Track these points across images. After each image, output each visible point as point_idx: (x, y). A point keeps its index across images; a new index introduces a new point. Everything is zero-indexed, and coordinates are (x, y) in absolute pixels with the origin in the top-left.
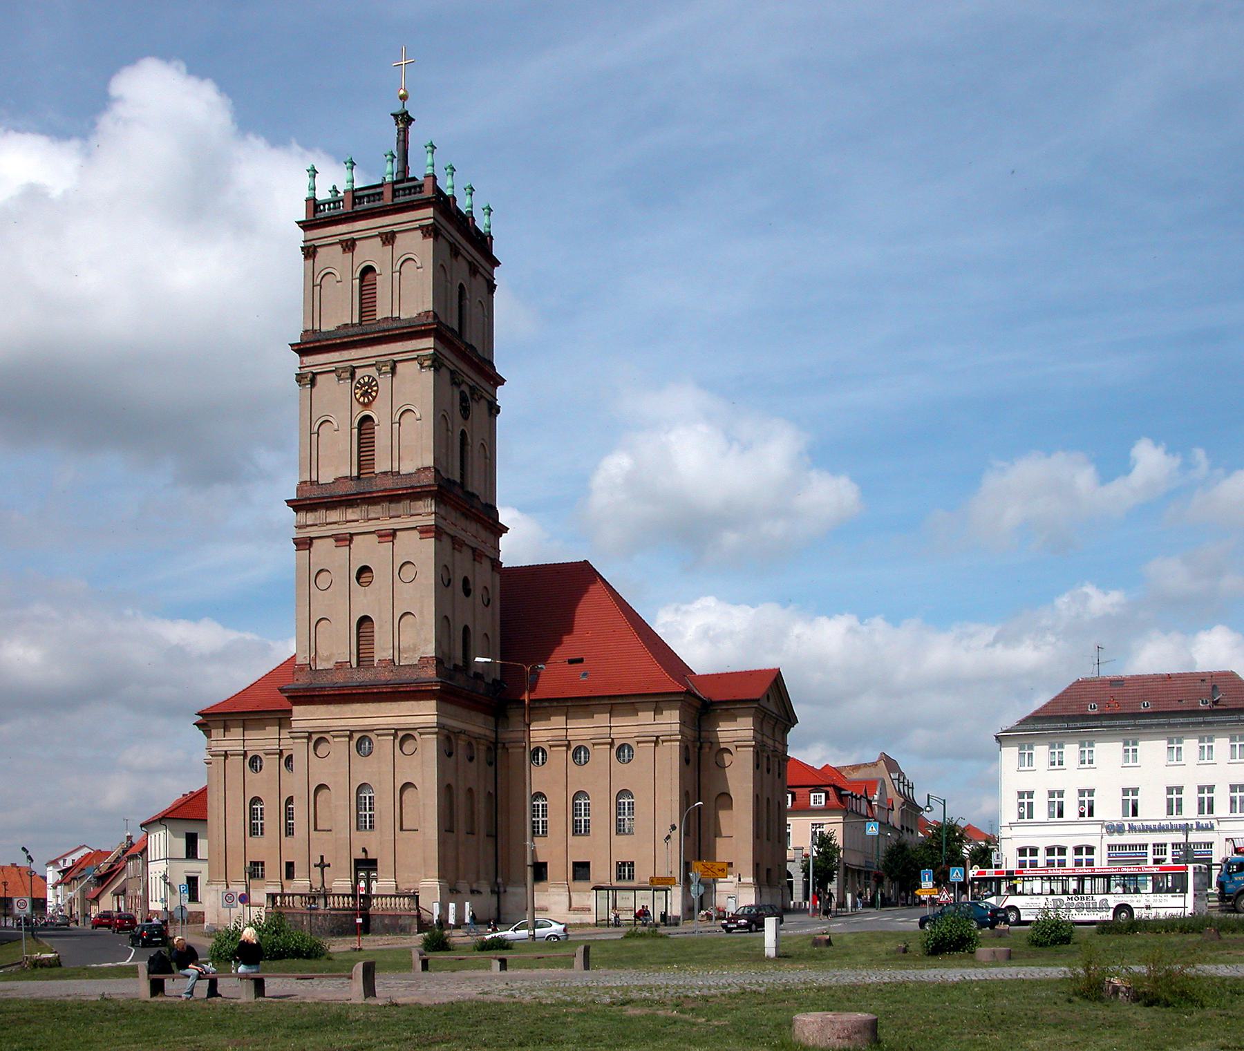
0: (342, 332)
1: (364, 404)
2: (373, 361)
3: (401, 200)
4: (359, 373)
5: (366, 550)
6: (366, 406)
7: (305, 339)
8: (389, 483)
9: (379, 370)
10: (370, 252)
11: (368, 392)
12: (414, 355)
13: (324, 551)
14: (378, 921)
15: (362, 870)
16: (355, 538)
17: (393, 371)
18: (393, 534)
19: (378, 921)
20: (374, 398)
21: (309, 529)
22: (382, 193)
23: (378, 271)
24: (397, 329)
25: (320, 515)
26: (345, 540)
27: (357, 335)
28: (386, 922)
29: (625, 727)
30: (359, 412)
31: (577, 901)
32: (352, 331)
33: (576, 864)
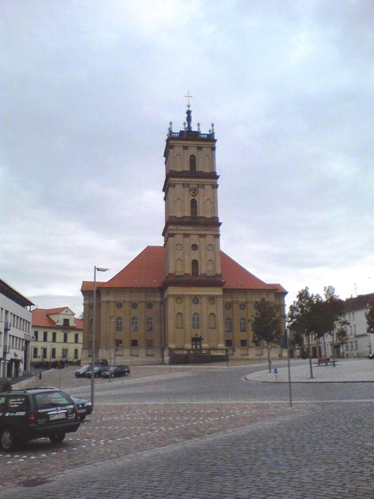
1: (193, 195)
4: (191, 186)
5: (194, 239)
11: (194, 192)
33: (133, 341)
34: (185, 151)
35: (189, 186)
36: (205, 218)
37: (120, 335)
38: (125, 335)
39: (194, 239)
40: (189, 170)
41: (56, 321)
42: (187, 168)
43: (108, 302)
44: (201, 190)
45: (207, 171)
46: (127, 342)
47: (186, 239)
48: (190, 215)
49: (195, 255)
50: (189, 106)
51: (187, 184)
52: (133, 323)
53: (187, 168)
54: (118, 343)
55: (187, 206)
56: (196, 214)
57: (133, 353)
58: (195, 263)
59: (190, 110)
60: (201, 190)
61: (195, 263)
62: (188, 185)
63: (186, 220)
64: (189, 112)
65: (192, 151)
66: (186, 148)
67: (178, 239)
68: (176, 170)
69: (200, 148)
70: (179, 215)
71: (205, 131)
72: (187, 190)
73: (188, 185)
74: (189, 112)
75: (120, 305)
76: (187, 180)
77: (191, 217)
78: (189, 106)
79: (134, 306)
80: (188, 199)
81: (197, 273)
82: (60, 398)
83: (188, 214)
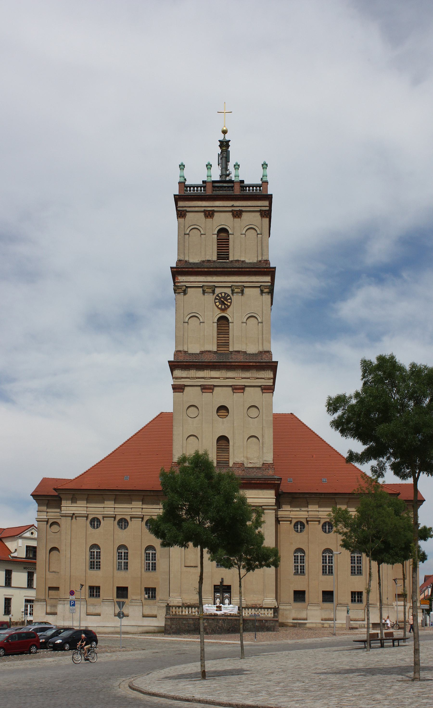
0: (206, 265)
1: (221, 309)
2: (230, 284)
3: (215, 193)
4: (218, 291)
5: (222, 396)
6: (223, 310)
7: (180, 266)
8: (241, 358)
9: (233, 291)
10: (223, 220)
11: (224, 302)
12: (258, 284)
13: (192, 395)
14: (250, 624)
15: (218, 592)
16: (246, 389)
17: (242, 292)
18: (242, 388)
19: (250, 624)
20: (229, 306)
21: (183, 380)
22: (232, 187)
23: (230, 232)
24: (220, 268)
25: (193, 373)
26: (210, 389)
27: (220, 268)
28: (257, 624)
29: (124, 509)
30: (218, 314)
31: (352, 615)
32: (212, 265)
33: (118, 588)
34: (209, 220)
35: (213, 292)
36: (245, 353)
37: (95, 578)
38: (108, 577)
39: (222, 396)
40: (215, 258)
41: (13, 551)
42: (211, 254)
43: (73, 516)
44: (236, 298)
45: (250, 258)
46: (108, 592)
47: (207, 396)
48: (215, 349)
49: (222, 427)
50: (225, 132)
51: (209, 287)
52: (120, 557)
53: (211, 254)
54: (95, 591)
55: (211, 329)
56: (227, 344)
57: (147, 612)
58: (223, 441)
59: (227, 139)
60: (236, 298)
61: (223, 441)
62: (213, 289)
63: (207, 358)
64: (224, 145)
65: (223, 220)
66: (209, 214)
67: (192, 395)
68: (191, 261)
69: (237, 214)
70: (194, 348)
71: (250, 176)
72: (210, 298)
73: (213, 289)
74: (224, 145)
75: (95, 522)
76: (209, 279)
77: (215, 353)
78: (225, 132)
79: (123, 523)
80: (212, 313)
81: (227, 462)
82: (134, 680)
83: (274, 511)
